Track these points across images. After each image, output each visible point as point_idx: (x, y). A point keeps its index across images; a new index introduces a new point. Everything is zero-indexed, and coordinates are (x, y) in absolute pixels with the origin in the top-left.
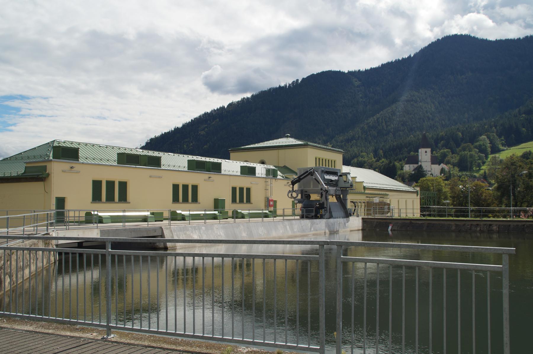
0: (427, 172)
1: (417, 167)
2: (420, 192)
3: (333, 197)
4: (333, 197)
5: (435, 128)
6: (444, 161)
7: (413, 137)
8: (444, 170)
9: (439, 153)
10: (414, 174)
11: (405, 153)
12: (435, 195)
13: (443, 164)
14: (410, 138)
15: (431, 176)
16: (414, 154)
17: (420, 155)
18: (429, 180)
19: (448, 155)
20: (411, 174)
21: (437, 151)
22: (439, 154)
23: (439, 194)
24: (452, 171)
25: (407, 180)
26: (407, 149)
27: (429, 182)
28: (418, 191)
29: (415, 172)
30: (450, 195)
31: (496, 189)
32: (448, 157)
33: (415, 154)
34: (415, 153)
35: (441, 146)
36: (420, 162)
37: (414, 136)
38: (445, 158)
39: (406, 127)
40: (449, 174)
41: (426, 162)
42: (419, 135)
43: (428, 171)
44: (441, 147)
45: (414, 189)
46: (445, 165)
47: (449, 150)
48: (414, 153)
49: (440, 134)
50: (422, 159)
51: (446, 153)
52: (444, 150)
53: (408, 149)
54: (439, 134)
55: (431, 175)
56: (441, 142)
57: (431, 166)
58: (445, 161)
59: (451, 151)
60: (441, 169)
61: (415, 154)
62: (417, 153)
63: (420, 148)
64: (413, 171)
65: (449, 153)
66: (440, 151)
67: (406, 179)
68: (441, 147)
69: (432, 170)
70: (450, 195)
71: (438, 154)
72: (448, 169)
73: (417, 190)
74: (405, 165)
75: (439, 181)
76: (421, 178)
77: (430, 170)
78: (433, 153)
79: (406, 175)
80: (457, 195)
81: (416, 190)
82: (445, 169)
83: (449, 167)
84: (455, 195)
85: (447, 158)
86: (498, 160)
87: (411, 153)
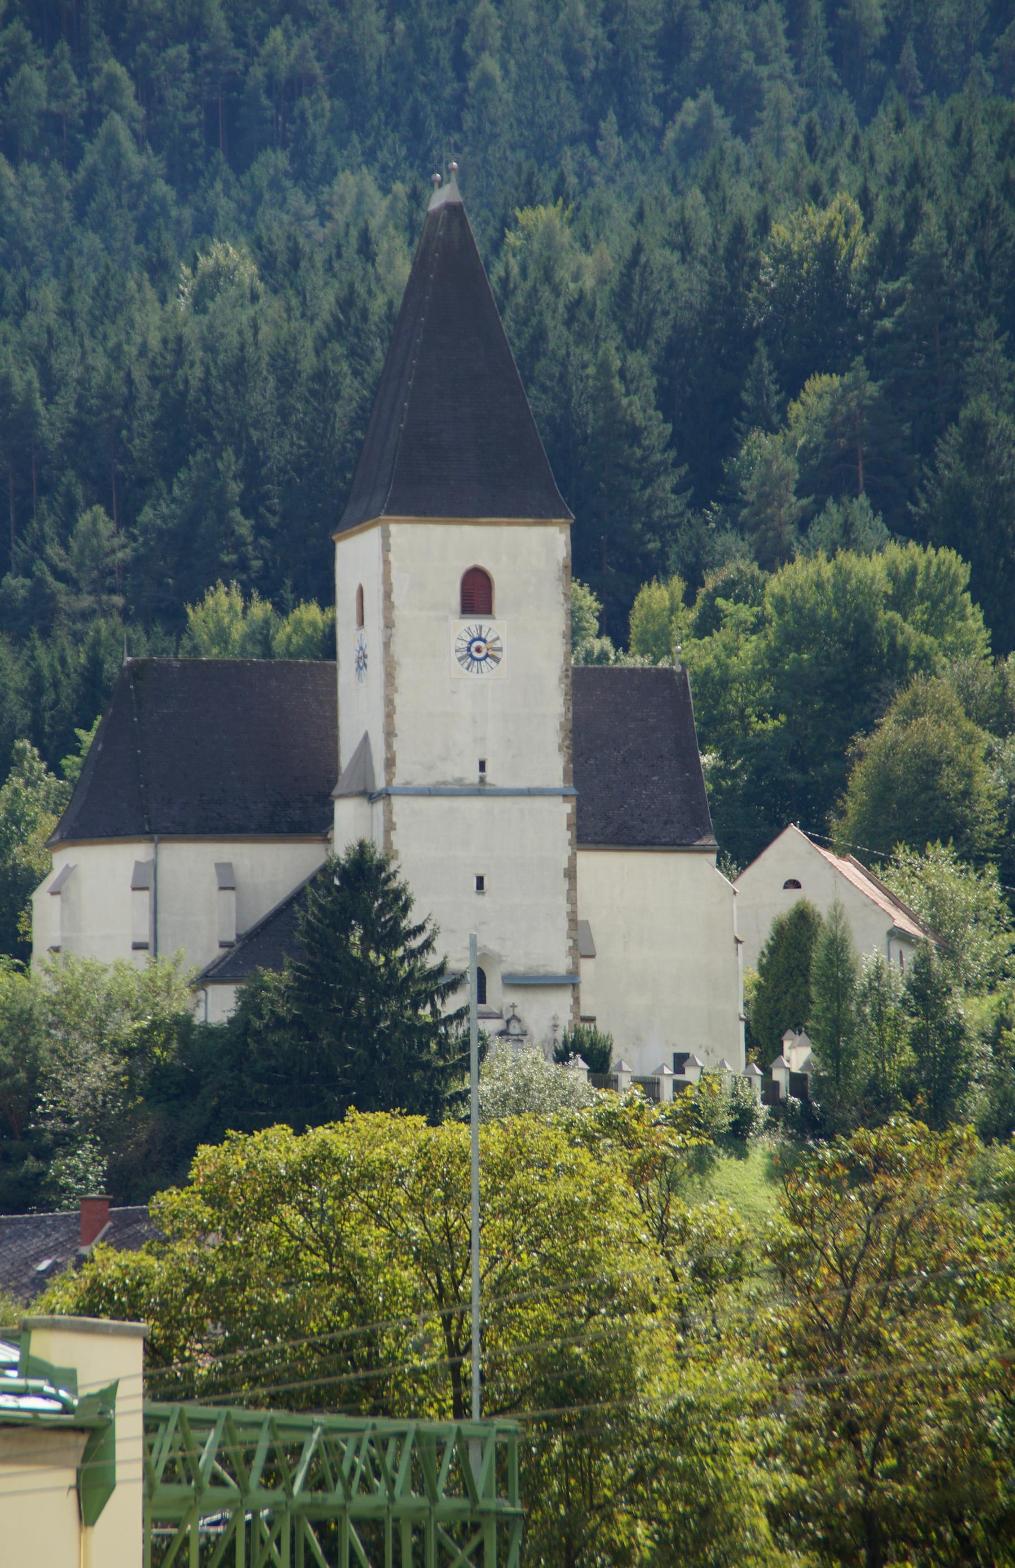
0: (497, 996)
1: (298, 897)
2: (151, 1425)
3: (137, 947)
4: (137, 947)
5: (690, 110)
6: (840, 783)
7: (248, 271)
8: (818, 954)
9: (746, 613)
10: (240, 1024)
11: (86, 601)
12: (482, 1473)
13: (820, 836)
14: (199, 306)
15: (578, 1072)
16: (262, 637)
17: (362, 662)
18: (368, 1177)
19: (924, 660)
20: (183, 1024)
21: (711, 582)
22: (750, 647)
23: (563, 1466)
24: (973, 988)
25: (86, 1152)
26: (125, 517)
27: (374, 1214)
28: (108, 1396)
29: (249, 1004)
30: (796, 1483)
31: (784, 1492)
32: (914, 711)
33: (283, 633)
34: (282, 609)
35: (790, 465)
36: (370, 796)
37: (267, 266)
38: (870, 727)
39: (114, 67)
40: (919, 1042)
41: (481, 790)
42: (366, 249)
43: (516, 982)
44: (794, 505)
45: (29, 1367)
46: (849, 869)
47: (949, 557)
48: (261, 609)
49: (780, 231)
50: (390, 733)
51: (885, 616)
52: (848, 560)
53: (147, 515)
54: (764, 223)
55: (561, 1057)
56: (793, 389)
57: (571, 874)
58: (858, 778)
59: (977, 589)
60: (762, 936)
61: (283, 633)
62: (310, 613)
63: (363, 520)
64: (208, 978)
65: (933, 626)
66: (775, 584)
67: (67, 1142)
68: (794, 505)
69: (587, 967)
70: (796, 1483)
71: (721, 637)
72: (897, 935)
73: (90, 1383)
74: (65, 858)
75: (563, 1188)
76: (216, 1139)
77: (560, 964)
78: (636, 619)
79: (75, 1068)
80: (938, 1479)
81: (67, 1378)
82: (837, 948)
83: (936, 901)
84: (897, 1490)
85: (889, 726)
86: (977, 1017)
87: (195, 615)
